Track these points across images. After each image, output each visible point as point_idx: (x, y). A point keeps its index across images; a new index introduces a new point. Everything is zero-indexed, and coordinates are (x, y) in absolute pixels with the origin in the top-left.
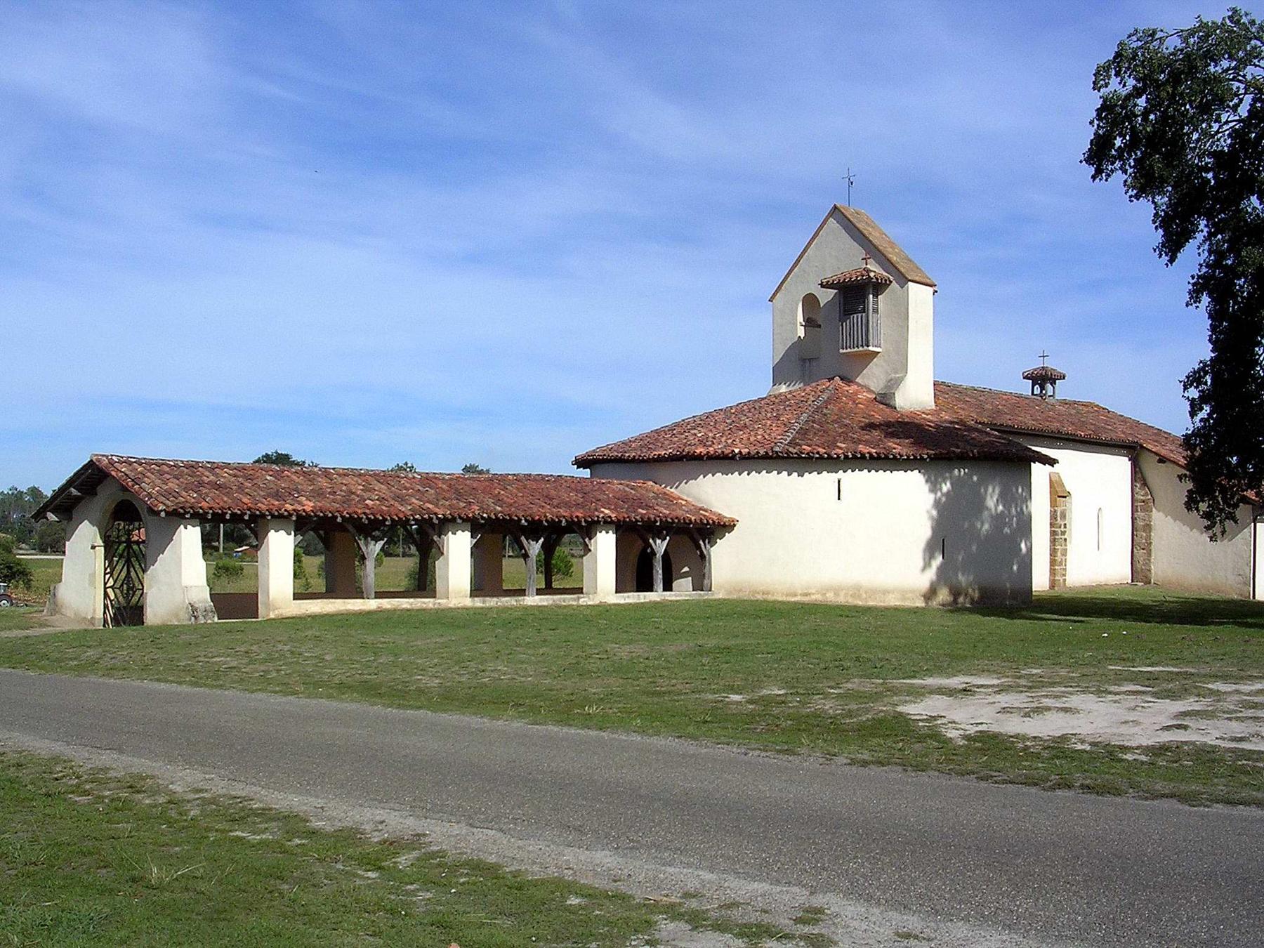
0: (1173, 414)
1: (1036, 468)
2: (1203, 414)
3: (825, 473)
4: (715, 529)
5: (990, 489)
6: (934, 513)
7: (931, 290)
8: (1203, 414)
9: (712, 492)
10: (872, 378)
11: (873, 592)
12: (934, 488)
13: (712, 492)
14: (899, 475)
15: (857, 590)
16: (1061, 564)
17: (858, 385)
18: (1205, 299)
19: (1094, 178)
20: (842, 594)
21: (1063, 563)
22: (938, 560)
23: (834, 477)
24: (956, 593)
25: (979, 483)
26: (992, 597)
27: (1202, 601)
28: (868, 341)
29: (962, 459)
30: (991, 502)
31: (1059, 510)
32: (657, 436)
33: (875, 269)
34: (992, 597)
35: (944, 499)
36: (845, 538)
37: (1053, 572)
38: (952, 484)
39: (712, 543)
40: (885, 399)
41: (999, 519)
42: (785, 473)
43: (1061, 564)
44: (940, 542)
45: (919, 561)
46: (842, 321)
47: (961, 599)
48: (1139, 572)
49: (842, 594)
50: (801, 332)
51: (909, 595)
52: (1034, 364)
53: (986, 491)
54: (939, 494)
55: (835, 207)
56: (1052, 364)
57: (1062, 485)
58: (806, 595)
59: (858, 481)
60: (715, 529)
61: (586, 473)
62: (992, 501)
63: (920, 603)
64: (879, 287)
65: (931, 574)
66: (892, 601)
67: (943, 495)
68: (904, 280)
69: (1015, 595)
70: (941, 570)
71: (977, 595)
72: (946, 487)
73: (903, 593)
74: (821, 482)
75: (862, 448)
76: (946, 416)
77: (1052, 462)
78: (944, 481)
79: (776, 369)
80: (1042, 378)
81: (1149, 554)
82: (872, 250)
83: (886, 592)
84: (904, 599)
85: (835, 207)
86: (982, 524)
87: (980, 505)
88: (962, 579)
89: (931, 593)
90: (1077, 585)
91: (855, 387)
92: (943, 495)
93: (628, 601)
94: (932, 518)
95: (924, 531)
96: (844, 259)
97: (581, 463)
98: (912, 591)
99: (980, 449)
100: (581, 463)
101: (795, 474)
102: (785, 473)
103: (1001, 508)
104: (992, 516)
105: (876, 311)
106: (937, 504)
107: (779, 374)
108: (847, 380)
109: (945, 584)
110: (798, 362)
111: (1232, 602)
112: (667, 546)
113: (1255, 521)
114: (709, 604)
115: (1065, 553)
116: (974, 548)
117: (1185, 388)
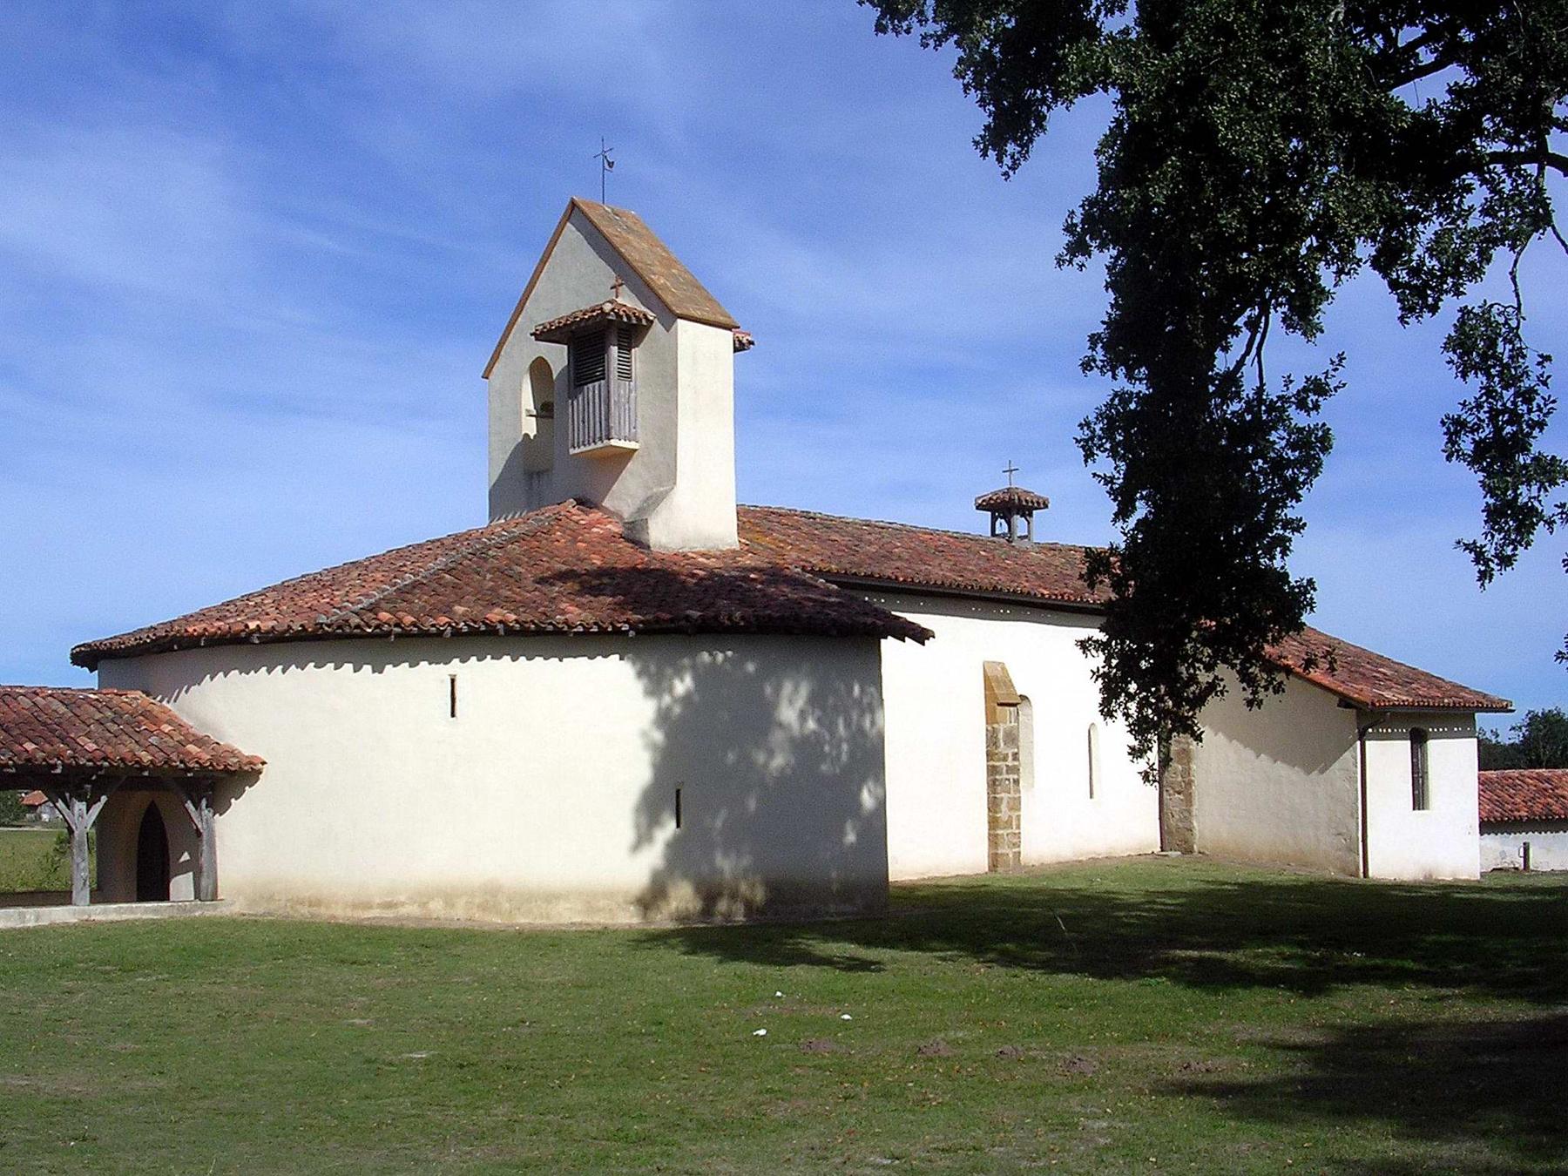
0: (1084, 514)
1: (889, 645)
2: (1141, 510)
3: (424, 664)
4: (223, 779)
5: (788, 687)
6: (658, 736)
7: (727, 337)
8: (1141, 510)
9: (229, 708)
10: (623, 497)
11: (526, 898)
12: (656, 686)
13: (229, 708)
14: (578, 667)
15: (491, 895)
16: (1008, 824)
17: (605, 510)
18: (1101, 260)
19: (880, 28)
20: (461, 903)
21: (1014, 823)
22: (667, 830)
23: (441, 672)
24: (709, 895)
25: (762, 676)
26: (787, 896)
27: (1252, 890)
28: (608, 428)
29: (710, 630)
30: (788, 714)
31: (1001, 729)
32: (223, 610)
33: (628, 301)
34: (787, 896)
35: (677, 710)
36: (514, 794)
37: (994, 840)
38: (696, 679)
39: (219, 806)
40: (634, 535)
41: (805, 748)
42: (348, 667)
43: (1008, 824)
44: (670, 794)
45: (624, 826)
46: (573, 396)
47: (722, 905)
48: (1174, 832)
49: (461, 903)
50: (530, 427)
51: (601, 903)
52: (994, 485)
53: (777, 691)
54: (667, 699)
55: (573, 204)
56: (1029, 484)
57: (1009, 684)
58: (389, 906)
59: (491, 679)
60: (223, 779)
61: (86, 679)
62: (792, 707)
63: (629, 918)
64: (630, 332)
65: (653, 856)
66: (566, 915)
67: (675, 700)
68: (670, 316)
69: (847, 892)
70: (677, 853)
71: (759, 895)
72: (683, 685)
73: (590, 898)
74: (416, 684)
75: (495, 615)
76: (747, 561)
77: (922, 635)
78: (679, 673)
79: (494, 494)
80: (1006, 507)
81: (1189, 800)
82: (627, 272)
83: (551, 897)
84: (590, 909)
85: (573, 204)
86: (771, 754)
87: (762, 720)
88: (726, 865)
89: (651, 899)
90: (1047, 860)
91: (596, 515)
92: (675, 700)
93: (114, 917)
94: (653, 747)
95: (637, 771)
96: (578, 285)
97: (87, 657)
98: (610, 895)
99: (810, 613)
100: (87, 657)
101: (367, 668)
102: (348, 667)
103: (811, 724)
104: (792, 740)
105: (626, 375)
106: (663, 718)
107: (499, 498)
108: (584, 503)
109: (685, 876)
110: (530, 475)
111: (1335, 883)
112: (158, 811)
113: (1362, 736)
114: (216, 923)
115: (1016, 805)
116: (752, 804)
117: (1089, 455)
